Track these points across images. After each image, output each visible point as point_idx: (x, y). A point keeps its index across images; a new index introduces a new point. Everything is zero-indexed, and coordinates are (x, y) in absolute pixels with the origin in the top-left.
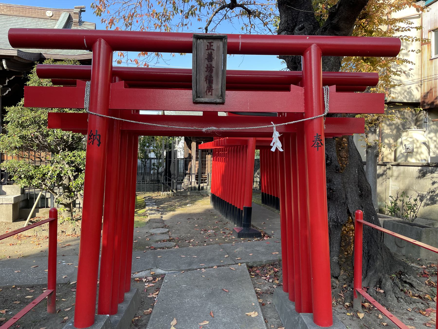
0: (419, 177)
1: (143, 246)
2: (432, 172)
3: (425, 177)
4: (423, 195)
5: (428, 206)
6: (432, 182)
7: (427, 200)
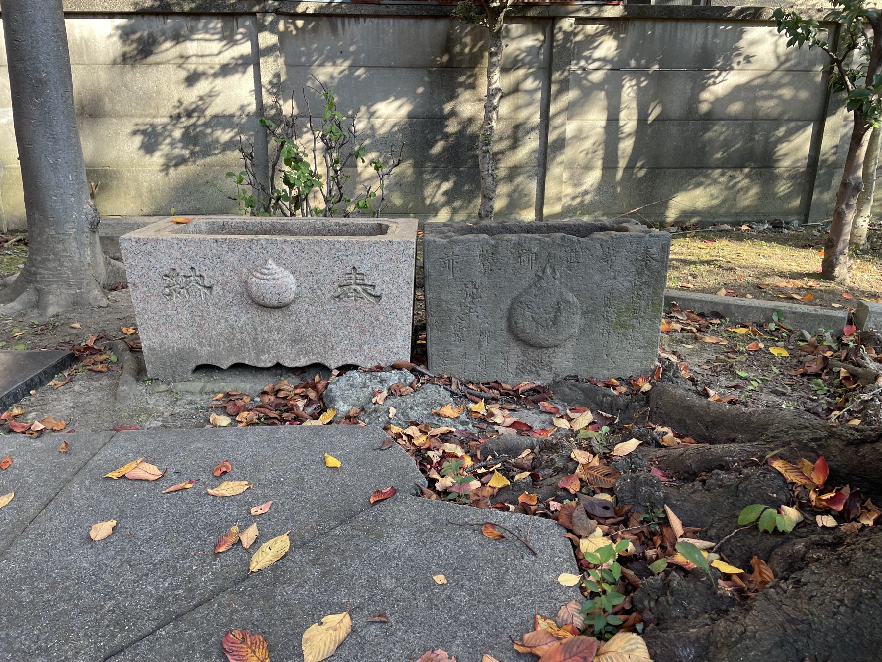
0: (125, 58)
1: (676, 27)
2: (178, 38)
3: (152, 59)
4: (154, 127)
5: (182, 168)
6: (183, 74)
7: (172, 144)
